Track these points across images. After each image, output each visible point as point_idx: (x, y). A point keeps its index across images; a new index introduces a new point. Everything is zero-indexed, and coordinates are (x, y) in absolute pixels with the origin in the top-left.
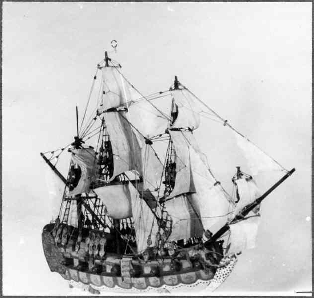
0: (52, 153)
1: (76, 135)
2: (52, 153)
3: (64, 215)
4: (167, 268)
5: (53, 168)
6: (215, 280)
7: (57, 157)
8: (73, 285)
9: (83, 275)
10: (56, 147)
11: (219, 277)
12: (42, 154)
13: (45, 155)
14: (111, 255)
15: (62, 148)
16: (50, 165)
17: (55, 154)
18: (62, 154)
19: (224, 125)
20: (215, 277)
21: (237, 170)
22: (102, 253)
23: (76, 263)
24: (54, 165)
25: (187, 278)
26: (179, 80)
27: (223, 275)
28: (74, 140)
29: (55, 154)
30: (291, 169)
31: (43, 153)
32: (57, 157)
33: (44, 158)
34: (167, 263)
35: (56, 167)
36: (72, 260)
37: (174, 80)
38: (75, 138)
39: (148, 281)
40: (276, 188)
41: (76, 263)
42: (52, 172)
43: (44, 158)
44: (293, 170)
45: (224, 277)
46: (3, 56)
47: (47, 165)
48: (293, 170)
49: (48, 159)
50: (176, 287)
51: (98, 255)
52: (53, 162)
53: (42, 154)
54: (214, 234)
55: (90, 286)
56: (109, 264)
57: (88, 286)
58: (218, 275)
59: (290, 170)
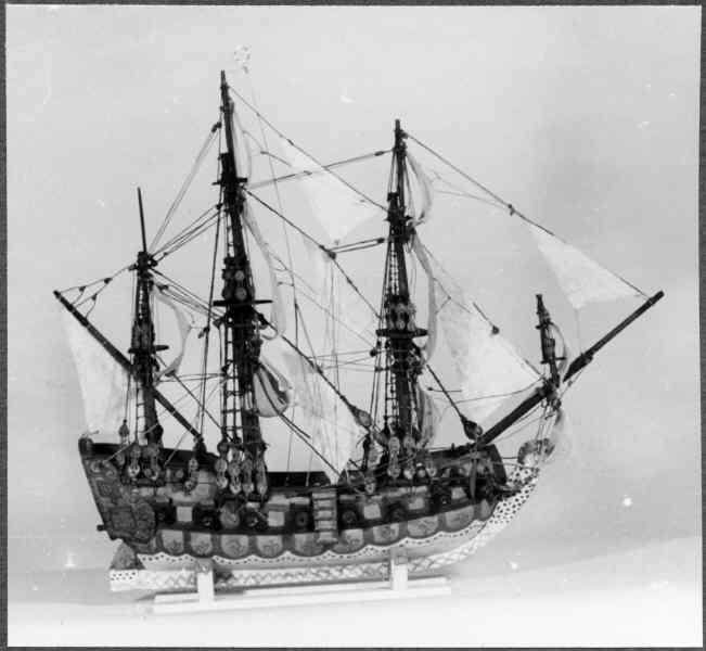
0: (82, 289)
1: (142, 249)
2: (82, 289)
3: (137, 418)
4: (418, 504)
5: (84, 321)
6: (496, 519)
7: (94, 298)
8: (144, 563)
9: (202, 539)
10: (91, 278)
11: (504, 511)
12: (57, 294)
13: (64, 295)
14: (279, 492)
15: (80, 285)
16: (78, 315)
17: (89, 293)
18: (105, 290)
19: (511, 214)
20: (496, 512)
21: (535, 301)
22: (262, 489)
23: (185, 515)
24: (84, 315)
25: (457, 519)
26: (402, 127)
27: (514, 506)
28: (134, 260)
29: (89, 293)
30: (656, 292)
31: (59, 290)
32: (94, 298)
33: (63, 301)
34: (419, 495)
35: (90, 319)
36: (174, 509)
37: (394, 127)
38: (140, 254)
39: (219, 543)
40: (631, 325)
41: (185, 515)
42: (83, 330)
43: (63, 301)
44: (660, 295)
45: (514, 512)
46: (116, 6)
47: (69, 315)
48: (660, 295)
49: (70, 301)
50: (428, 542)
51: (402, 476)
52: (82, 311)
53: (57, 294)
54: (485, 429)
55: (214, 561)
56: (277, 508)
57: (207, 562)
58: (504, 508)
59: (653, 295)
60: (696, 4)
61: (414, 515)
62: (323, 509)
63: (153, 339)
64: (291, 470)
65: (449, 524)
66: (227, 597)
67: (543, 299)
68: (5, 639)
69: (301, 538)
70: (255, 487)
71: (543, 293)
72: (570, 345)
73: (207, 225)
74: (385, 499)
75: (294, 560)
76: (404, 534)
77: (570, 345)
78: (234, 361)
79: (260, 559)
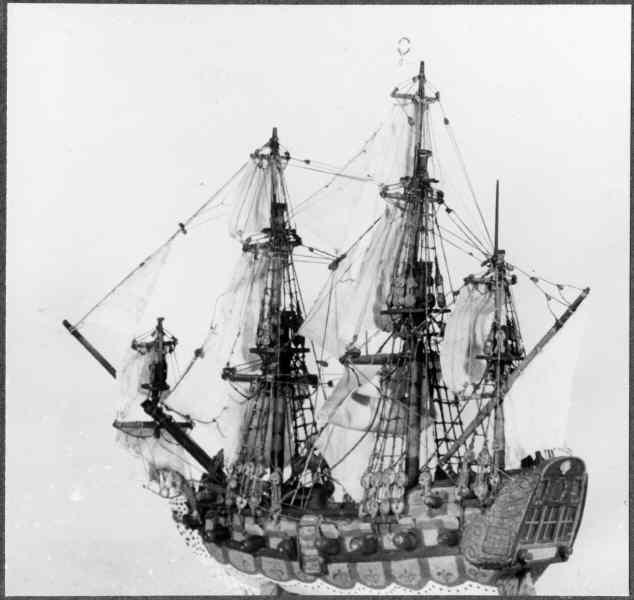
2: (549, 298)
61: (433, 551)
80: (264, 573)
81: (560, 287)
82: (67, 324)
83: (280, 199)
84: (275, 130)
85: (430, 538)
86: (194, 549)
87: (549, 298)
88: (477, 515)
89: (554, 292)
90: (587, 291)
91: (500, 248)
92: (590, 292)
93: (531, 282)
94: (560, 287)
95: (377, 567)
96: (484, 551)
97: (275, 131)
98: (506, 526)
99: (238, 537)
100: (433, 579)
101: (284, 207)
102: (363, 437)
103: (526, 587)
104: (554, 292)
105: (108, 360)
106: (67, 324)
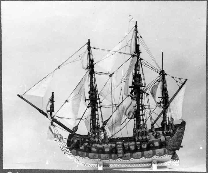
2: (177, 82)
15: (176, 82)
36: (104, 149)
60: (1, 2)
61: (157, 148)
62: (120, 147)
63: (76, 131)
64: (129, 136)
65: (145, 155)
66: (146, 168)
67: (54, 94)
68: (2, 167)
69: (113, 155)
70: (146, 137)
71: (54, 92)
72: (45, 108)
73: (151, 66)
74: (111, 146)
75: (157, 157)
76: (154, 154)
77: (45, 108)
78: (92, 123)
79: (134, 159)
80: (145, 157)
81: (180, 79)
82: (19, 95)
83: (138, 44)
84: (89, 40)
85: (157, 144)
86: (67, 155)
87: (177, 82)
88: (169, 138)
89: (178, 80)
90: (187, 79)
91: (163, 69)
92: (188, 80)
93: (172, 78)
94: (180, 79)
95: (140, 153)
96: (173, 146)
97: (89, 40)
98: (178, 139)
99: (94, 149)
100: (156, 155)
101: (139, 45)
102: (129, 121)
103: (135, 156)
104: (178, 80)
105: (35, 105)
106: (19, 95)
